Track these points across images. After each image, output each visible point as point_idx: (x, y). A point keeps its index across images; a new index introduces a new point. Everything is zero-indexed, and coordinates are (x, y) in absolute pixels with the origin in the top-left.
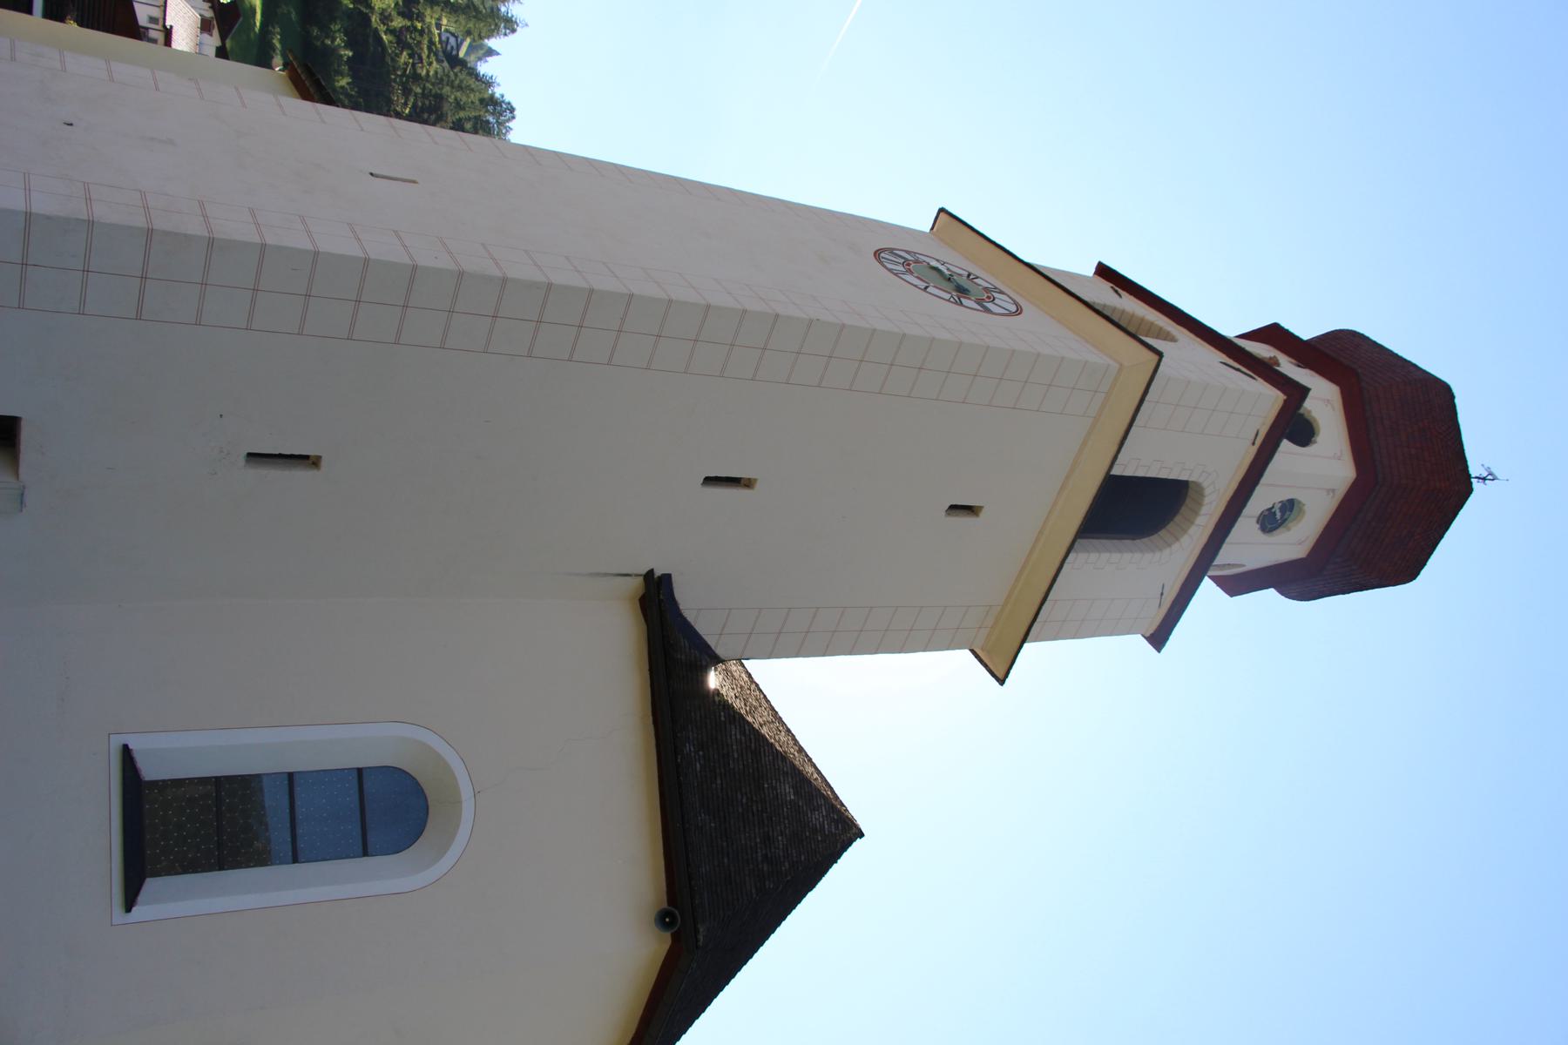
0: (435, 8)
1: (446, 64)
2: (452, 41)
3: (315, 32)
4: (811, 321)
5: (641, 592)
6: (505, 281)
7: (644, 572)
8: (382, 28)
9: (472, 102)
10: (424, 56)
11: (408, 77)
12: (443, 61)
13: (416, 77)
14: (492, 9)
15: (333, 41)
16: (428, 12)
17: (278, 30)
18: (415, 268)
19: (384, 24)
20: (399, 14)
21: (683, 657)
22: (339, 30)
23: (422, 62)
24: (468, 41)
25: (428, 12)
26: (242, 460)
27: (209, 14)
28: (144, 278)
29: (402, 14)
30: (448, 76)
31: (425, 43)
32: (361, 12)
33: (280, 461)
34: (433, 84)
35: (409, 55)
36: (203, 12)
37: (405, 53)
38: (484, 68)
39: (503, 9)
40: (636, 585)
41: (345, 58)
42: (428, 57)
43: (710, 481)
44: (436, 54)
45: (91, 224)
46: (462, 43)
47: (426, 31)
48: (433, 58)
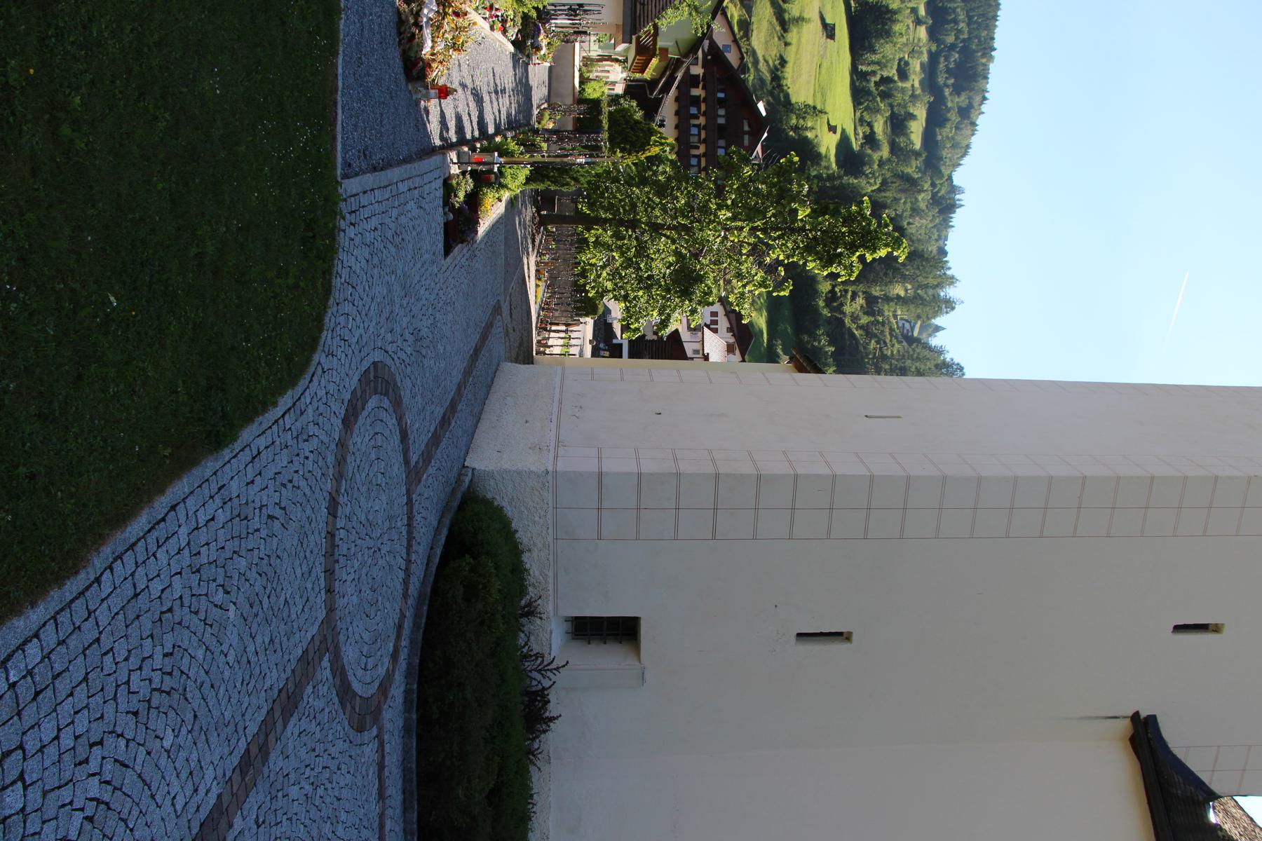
0: (891, 304)
1: (905, 344)
2: (907, 325)
3: (806, 338)
4: (1249, 479)
5: (1130, 732)
6: (979, 479)
7: (1130, 714)
8: (854, 326)
9: (930, 369)
10: (888, 341)
11: (878, 359)
12: (902, 342)
13: (884, 357)
14: (933, 295)
15: (819, 343)
16: (886, 307)
17: (780, 342)
18: (909, 478)
19: (855, 323)
20: (864, 313)
21: (1179, 792)
22: (823, 334)
23: (886, 346)
24: (919, 322)
25: (886, 307)
26: (793, 639)
27: (732, 340)
28: (715, 509)
29: (867, 313)
30: (908, 352)
31: (887, 331)
32: (837, 318)
33: (822, 638)
34: (897, 360)
35: (876, 342)
36: (728, 340)
37: (873, 341)
38: (935, 341)
39: (942, 294)
40: (1125, 727)
41: (830, 353)
42: (891, 341)
43: (1179, 628)
44: (896, 338)
45: (678, 475)
46: (914, 326)
47: (887, 322)
48: (895, 341)
